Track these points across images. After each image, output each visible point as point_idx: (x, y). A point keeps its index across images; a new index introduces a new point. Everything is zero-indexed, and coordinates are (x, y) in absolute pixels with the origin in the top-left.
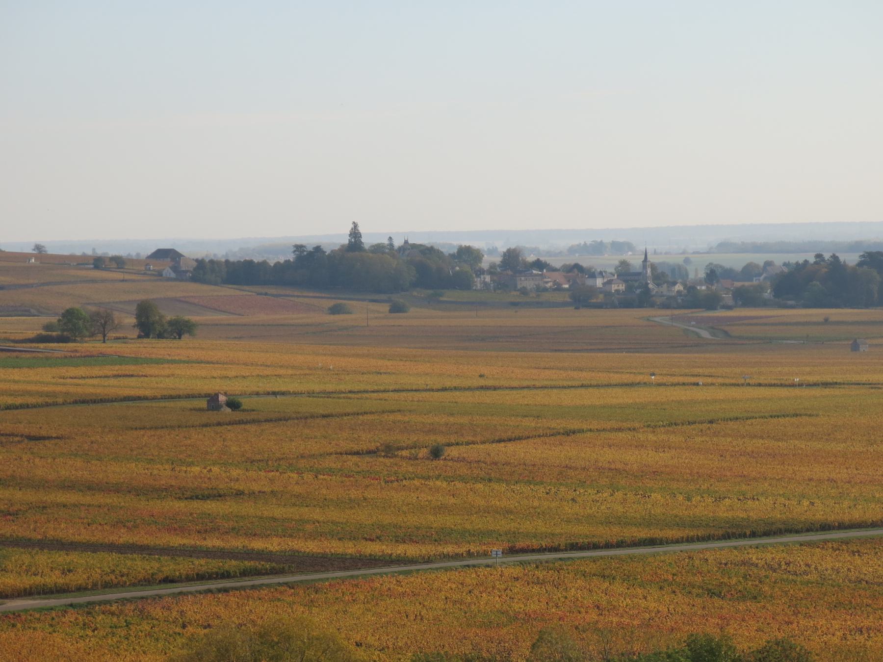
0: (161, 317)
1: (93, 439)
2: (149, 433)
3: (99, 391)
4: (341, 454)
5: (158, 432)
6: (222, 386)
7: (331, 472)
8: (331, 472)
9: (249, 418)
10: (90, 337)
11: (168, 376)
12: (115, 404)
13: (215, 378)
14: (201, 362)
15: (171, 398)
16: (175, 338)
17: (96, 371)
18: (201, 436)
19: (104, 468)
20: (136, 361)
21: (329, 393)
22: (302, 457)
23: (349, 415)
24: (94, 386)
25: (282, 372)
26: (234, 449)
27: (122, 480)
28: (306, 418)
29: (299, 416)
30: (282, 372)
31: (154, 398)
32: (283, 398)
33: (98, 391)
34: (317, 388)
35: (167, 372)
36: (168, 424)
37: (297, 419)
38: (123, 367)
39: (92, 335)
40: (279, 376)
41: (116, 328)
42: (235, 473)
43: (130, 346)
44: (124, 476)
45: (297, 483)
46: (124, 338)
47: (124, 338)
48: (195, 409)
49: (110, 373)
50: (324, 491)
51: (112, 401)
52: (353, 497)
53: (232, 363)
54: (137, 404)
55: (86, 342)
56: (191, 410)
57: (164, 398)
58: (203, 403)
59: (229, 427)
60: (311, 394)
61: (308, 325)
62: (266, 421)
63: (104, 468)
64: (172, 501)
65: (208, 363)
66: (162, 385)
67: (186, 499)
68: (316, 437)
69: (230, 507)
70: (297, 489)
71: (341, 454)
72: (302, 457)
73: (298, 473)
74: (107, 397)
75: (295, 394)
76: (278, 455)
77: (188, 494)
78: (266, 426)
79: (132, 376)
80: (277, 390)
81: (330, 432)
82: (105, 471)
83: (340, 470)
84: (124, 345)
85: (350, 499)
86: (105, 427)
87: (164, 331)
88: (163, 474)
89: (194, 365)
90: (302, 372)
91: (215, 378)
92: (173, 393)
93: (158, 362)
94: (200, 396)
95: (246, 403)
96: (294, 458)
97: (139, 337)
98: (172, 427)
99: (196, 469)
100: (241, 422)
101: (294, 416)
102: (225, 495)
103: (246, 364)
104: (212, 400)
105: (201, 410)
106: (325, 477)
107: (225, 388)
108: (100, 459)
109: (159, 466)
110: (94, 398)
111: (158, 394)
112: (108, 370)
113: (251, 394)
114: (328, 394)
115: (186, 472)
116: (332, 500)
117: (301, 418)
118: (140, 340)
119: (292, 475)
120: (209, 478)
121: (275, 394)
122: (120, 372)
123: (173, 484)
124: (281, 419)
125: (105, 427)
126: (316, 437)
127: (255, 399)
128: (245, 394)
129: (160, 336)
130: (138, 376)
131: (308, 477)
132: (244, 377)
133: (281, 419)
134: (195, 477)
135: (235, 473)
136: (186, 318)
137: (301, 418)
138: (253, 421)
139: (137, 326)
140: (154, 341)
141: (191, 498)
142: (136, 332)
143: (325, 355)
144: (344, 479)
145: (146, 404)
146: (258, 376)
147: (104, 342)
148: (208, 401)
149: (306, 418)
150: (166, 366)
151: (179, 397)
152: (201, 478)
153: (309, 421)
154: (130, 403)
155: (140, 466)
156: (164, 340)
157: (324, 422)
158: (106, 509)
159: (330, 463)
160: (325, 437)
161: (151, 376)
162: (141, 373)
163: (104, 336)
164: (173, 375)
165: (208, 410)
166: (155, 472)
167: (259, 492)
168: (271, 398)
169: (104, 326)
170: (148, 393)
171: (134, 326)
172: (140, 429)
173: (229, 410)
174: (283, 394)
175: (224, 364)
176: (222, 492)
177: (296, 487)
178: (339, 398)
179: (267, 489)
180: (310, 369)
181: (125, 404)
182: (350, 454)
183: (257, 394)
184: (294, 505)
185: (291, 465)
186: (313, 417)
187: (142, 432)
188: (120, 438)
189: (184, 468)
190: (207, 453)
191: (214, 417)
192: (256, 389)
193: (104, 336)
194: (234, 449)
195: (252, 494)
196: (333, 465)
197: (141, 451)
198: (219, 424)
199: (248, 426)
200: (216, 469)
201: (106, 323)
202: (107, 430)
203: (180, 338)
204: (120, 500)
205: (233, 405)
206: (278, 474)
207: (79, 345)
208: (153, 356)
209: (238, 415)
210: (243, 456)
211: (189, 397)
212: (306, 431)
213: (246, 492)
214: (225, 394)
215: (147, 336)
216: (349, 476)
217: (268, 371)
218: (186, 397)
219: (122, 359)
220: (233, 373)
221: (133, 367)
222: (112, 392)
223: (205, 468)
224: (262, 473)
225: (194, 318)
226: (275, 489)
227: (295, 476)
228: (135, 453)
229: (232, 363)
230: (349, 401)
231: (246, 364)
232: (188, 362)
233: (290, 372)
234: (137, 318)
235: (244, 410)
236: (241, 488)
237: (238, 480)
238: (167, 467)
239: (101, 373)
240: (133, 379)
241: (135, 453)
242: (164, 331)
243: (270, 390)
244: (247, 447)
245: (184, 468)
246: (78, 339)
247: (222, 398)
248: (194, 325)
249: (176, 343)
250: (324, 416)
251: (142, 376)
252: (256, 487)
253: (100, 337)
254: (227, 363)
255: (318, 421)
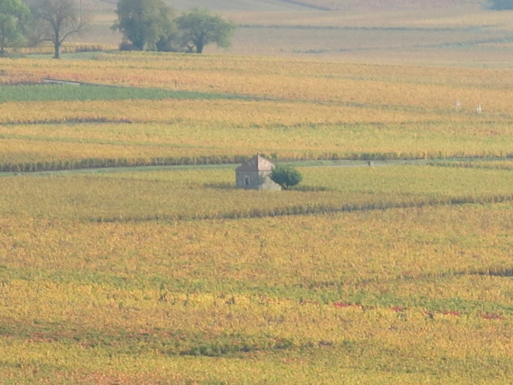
0: (164, 11)
1: (17, 238)
2: (122, 229)
3: (37, 148)
4: (481, 273)
5: (140, 228)
6: (266, 143)
7: (459, 308)
8: (459, 308)
9: (313, 203)
10: (29, 46)
11: (170, 123)
12: (65, 173)
13: (257, 127)
14: (236, 96)
15: (170, 162)
16: (190, 50)
17: (36, 111)
18: (219, 236)
19: (33, 293)
20: (113, 92)
21: (471, 158)
22: (407, 277)
23: (502, 199)
24: (29, 139)
25: (385, 116)
26: (279, 261)
27: (64, 318)
28: (421, 205)
29: (407, 200)
30: (385, 116)
31: (139, 164)
32: (382, 165)
33: (36, 149)
34: (447, 147)
35: (170, 114)
36: (160, 212)
37: (405, 206)
38: (88, 104)
39: (34, 42)
40: (379, 125)
41: (79, 31)
42: (277, 306)
43: (102, 64)
44: (69, 309)
45: (393, 328)
46: (94, 50)
47: (94, 50)
48: (212, 186)
49: (60, 115)
50: (443, 343)
51: (60, 168)
52: (496, 355)
53: (292, 99)
54: (108, 173)
55: (22, 56)
56: (206, 186)
57: (157, 163)
58: (228, 175)
59: (274, 221)
60: (435, 160)
61: (449, 29)
62: (346, 209)
63: (33, 293)
64: (155, 357)
65: (248, 98)
66: (156, 139)
67: (182, 354)
68: (435, 241)
69: (264, 370)
70: (393, 339)
71: (481, 273)
72: (407, 277)
73: (396, 309)
74: (50, 161)
75: (406, 158)
76: (362, 274)
77: (187, 345)
78: (343, 219)
79: (103, 120)
80: (371, 151)
81: (463, 232)
82: (35, 300)
83: (477, 304)
84: (92, 63)
85: (491, 360)
86: (40, 216)
87: (170, 38)
88: (144, 306)
89: (221, 102)
90: (423, 118)
91: (257, 127)
92: (175, 154)
93: (154, 95)
94: (225, 161)
95: (309, 175)
96: (391, 280)
97: (124, 47)
98: (167, 219)
99: (206, 299)
100: (297, 211)
101: (399, 200)
102: (255, 348)
103: (318, 102)
104: (246, 171)
105: (224, 187)
106: (448, 317)
107: (275, 147)
108: (27, 277)
109: (136, 291)
110: (27, 161)
111: (147, 156)
112: (58, 110)
113: (322, 159)
114: (466, 160)
115: (185, 303)
116: (457, 360)
117: (412, 205)
118: (125, 54)
119: (385, 312)
120: (229, 316)
121: (366, 158)
122: (80, 114)
123: (160, 325)
124: (370, 207)
125: (40, 216)
126: (435, 241)
127: (329, 167)
128: (311, 157)
129: (163, 46)
130: (114, 121)
131: (416, 316)
132: (313, 126)
133: (370, 207)
134: (202, 314)
135: (277, 306)
136: (212, 14)
137: (412, 205)
138: (322, 210)
139: (120, 27)
140: (150, 55)
141: (192, 353)
142: (118, 38)
143: (470, 85)
144: (483, 320)
145: (124, 173)
146: (340, 123)
147: (57, 56)
148: (238, 170)
149: (421, 205)
150: (167, 103)
151: (186, 162)
152: (213, 315)
153: (425, 210)
154: (93, 173)
155: (100, 291)
156: (170, 55)
157: (455, 212)
158: (30, 371)
159: (459, 290)
160: (454, 242)
161: (138, 122)
162: (119, 116)
163: (57, 45)
164: (179, 120)
165: (237, 187)
166: (129, 302)
167: (322, 343)
168: (360, 166)
169: (57, 27)
170: (128, 154)
171: (114, 28)
172: (107, 221)
173: (277, 188)
174: (383, 158)
175: (277, 100)
176: (250, 343)
177: (390, 335)
178: (486, 167)
179: (337, 338)
180: (440, 113)
181: (82, 174)
182: (499, 274)
183: (334, 158)
184: (385, 368)
185: (384, 292)
186: (433, 202)
187: (110, 227)
188: (69, 236)
189: (184, 297)
190: (227, 268)
191: (247, 199)
192: (332, 149)
193: (57, 45)
194: (279, 261)
195: (307, 346)
196: (464, 295)
197: (104, 263)
198: (256, 214)
199: (309, 219)
200: (243, 299)
201: (60, 20)
202: (44, 222)
203: (199, 51)
204: (58, 354)
205: (285, 179)
206: (359, 310)
207: (8, 60)
208: (146, 84)
209: (293, 198)
210: (296, 274)
211: (203, 161)
212: (420, 230)
213: (297, 343)
214: (273, 158)
215: (138, 46)
216: (494, 316)
217: (359, 116)
218: (199, 163)
219: (86, 90)
220: (294, 119)
221: (105, 105)
222: (59, 151)
223: (223, 297)
224: (330, 309)
225: (226, 16)
226: (352, 338)
227: (391, 314)
228: (94, 265)
229: (292, 99)
230: (505, 173)
231: (318, 102)
232: (209, 97)
233: (401, 117)
234: (118, 12)
235: (304, 189)
236: (287, 336)
237: (282, 319)
238: (151, 293)
239: (43, 115)
240: (105, 127)
241: (94, 265)
242: (170, 38)
243: (358, 150)
244: (305, 258)
245: (184, 297)
246: (9, 50)
247: (265, 166)
248: (226, 27)
249: (193, 59)
250: (455, 202)
251: (122, 121)
252: (315, 335)
253: (49, 46)
254: (283, 99)
255: (442, 210)
